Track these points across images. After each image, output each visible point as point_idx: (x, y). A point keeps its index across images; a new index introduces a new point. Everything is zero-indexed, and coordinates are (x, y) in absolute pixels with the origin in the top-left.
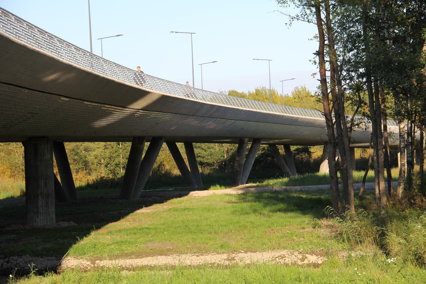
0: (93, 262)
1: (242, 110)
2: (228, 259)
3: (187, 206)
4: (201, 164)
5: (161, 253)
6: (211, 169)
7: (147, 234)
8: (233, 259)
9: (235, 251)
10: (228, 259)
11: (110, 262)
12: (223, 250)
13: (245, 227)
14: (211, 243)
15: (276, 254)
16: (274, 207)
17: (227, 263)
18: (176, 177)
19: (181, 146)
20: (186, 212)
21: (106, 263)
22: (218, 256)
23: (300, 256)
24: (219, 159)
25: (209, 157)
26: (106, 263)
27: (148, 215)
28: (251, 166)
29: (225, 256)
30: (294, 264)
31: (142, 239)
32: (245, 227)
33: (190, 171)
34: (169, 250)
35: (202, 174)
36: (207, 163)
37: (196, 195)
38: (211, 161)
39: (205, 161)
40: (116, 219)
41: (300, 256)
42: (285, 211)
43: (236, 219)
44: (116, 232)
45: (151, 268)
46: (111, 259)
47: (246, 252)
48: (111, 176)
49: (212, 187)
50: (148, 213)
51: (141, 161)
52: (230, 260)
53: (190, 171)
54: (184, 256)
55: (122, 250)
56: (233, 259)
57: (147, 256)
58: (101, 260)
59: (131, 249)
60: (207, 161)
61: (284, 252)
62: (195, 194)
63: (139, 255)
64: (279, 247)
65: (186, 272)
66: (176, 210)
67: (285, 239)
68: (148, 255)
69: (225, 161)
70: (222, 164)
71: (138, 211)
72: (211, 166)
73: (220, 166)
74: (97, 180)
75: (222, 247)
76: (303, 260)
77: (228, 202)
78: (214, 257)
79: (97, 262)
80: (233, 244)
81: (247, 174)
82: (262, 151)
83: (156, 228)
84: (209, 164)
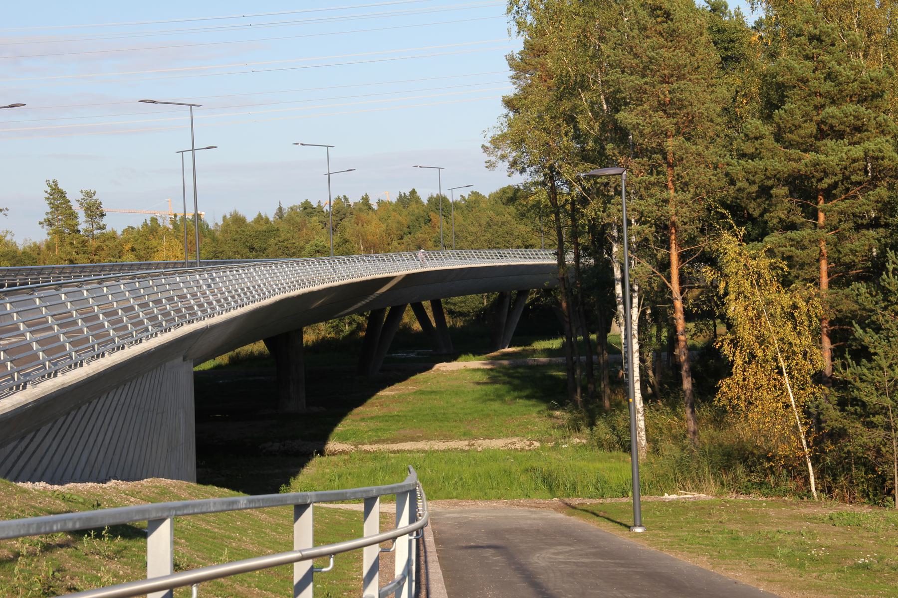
0: (356, 447)
1: (500, 267)
2: (469, 445)
3: (434, 388)
4: (451, 313)
5: (413, 439)
6: (465, 321)
7: (398, 421)
8: (473, 445)
9: (476, 438)
10: (469, 445)
11: (371, 446)
12: (465, 438)
13: (488, 415)
14: (455, 430)
15: (509, 441)
16: (516, 394)
17: (467, 448)
18: (417, 334)
19: (426, 304)
20: (433, 396)
21: (368, 447)
22: (461, 442)
23: (528, 443)
24: (477, 307)
25: (463, 305)
26: (368, 447)
27: (394, 399)
28: (515, 326)
29: (466, 443)
30: (522, 449)
31: (394, 427)
32: (488, 415)
33: (434, 325)
34: (419, 437)
35: (453, 328)
36: (459, 312)
37: (444, 369)
38: (465, 310)
39: (458, 310)
40: (360, 402)
41: (528, 443)
42: (528, 397)
43: (481, 406)
44: (369, 419)
45: (402, 451)
46: (371, 444)
47: (484, 439)
48: (333, 335)
49: (463, 357)
50: (394, 396)
51: (382, 326)
52: (471, 446)
53: (434, 325)
54: (432, 442)
55: (379, 437)
56: (473, 445)
57: (401, 442)
58: (363, 445)
59: (386, 435)
60: (461, 310)
61: (515, 439)
62: (443, 367)
63: (394, 441)
64: (514, 434)
65: (435, 455)
66: (422, 392)
67: (521, 427)
68: (402, 441)
69: (484, 309)
70: (480, 312)
71: (382, 393)
72: (465, 316)
73: (478, 316)
74: (317, 341)
75: (465, 434)
76: (530, 446)
77: (478, 383)
78: (458, 443)
79: (360, 446)
80: (475, 432)
81: (510, 334)
82: (537, 294)
83: (405, 416)
84: (461, 314)
